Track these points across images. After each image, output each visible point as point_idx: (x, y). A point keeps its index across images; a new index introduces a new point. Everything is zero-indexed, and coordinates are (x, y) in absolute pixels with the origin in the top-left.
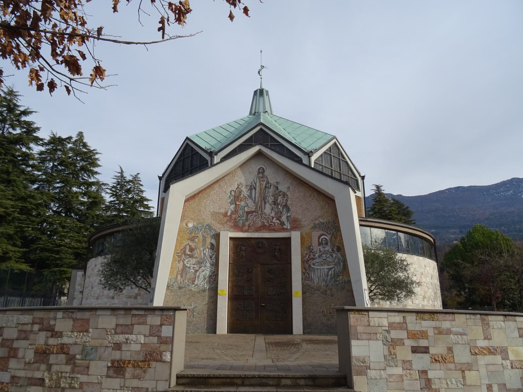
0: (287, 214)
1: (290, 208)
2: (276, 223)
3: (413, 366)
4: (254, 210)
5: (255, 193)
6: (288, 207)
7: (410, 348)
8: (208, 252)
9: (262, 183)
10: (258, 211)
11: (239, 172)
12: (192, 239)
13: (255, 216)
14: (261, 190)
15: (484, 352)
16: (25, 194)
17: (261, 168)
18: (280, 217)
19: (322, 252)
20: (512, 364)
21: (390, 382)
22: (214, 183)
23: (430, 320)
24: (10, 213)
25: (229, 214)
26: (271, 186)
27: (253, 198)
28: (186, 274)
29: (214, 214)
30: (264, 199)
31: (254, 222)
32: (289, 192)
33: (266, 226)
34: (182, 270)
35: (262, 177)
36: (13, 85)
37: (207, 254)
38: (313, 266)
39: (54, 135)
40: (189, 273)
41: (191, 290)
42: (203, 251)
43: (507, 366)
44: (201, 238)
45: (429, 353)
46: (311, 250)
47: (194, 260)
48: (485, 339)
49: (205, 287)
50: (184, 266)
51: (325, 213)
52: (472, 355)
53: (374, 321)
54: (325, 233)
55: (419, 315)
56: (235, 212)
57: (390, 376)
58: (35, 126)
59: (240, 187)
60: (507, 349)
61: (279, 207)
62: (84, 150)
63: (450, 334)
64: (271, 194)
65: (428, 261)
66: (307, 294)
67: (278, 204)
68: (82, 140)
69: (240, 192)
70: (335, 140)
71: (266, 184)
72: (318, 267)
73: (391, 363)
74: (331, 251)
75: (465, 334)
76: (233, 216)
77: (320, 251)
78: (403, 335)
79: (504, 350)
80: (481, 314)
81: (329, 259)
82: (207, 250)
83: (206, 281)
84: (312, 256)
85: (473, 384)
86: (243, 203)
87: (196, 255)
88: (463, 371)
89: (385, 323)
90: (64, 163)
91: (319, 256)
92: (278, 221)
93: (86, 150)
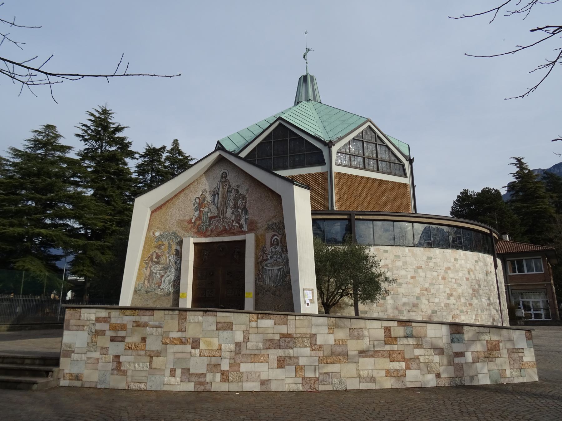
0: (246, 216)
1: (248, 210)
2: (236, 227)
3: (109, 352)
4: (216, 215)
5: (218, 198)
6: (247, 209)
7: (109, 337)
8: (173, 258)
9: (225, 187)
10: (220, 216)
11: (204, 179)
12: (159, 247)
13: (218, 220)
14: (223, 195)
15: (175, 342)
16: (122, 208)
17: (224, 172)
18: (240, 220)
19: (273, 253)
20: (201, 352)
21: (88, 363)
22: (180, 192)
23: (131, 315)
24: (108, 226)
25: (193, 221)
26: (232, 189)
27: (216, 203)
28: (153, 280)
29: (180, 222)
30: (226, 203)
31: (216, 227)
32: (247, 195)
33: (226, 229)
34: (149, 276)
35: (225, 182)
36: (106, 104)
37: (172, 260)
38: (265, 267)
39: (149, 146)
40: (155, 278)
41: (157, 294)
42: (169, 257)
43: (195, 354)
44: (167, 245)
45: (124, 342)
46: (264, 251)
47: (160, 266)
48: (179, 331)
49: (170, 290)
50: (151, 272)
51: (278, 213)
52: (163, 344)
53: (84, 316)
54: (277, 234)
55: (123, 311)
56: (199, 218)
57: (89, 358)
58: (126, 141)
59: (204, 193)
60: (200, 340)
61: (239, 210)
62: (180, 157)
63: (146, 327)
64: (232, 198)
65: (464, 255)
66: (260, 295)
67: (238, 207)
68: (178, 148)
69: (204, 199)
70: (369, 124)
71: (228, 189)
72: (270, 268)
73: (91, 348)
74: (281, 252)
75: (160, 327)
76: (197, 222)
77: (272, 252)
78: (106, 327)
79: (196, 341)
80: (203, 311)
81: (278, 260)
82: (172, 256)
83: (171, 285)
84: (265, 257)
85: (158, 368)
86: (206, 209)
87: (162, 262)
88: (151, 357)
89: (93, 317)
90: (159, 173)
91: (271, 257)
92: (237, 225)
93: (182, 158)
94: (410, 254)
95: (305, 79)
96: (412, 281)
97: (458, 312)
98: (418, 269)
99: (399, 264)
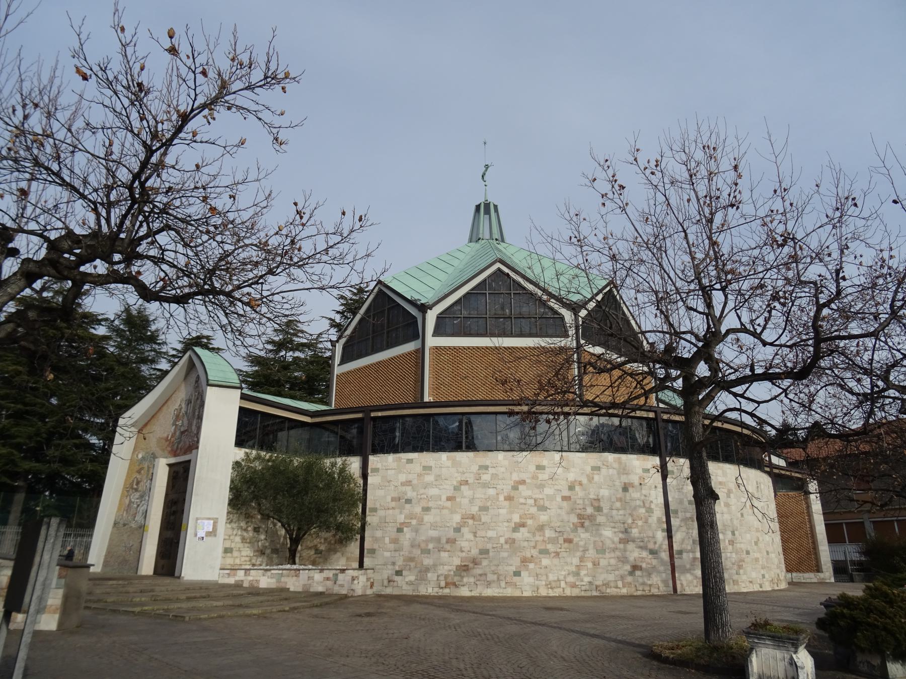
12: (139, 472)
65: (448, 458)
94: (449, 463)
95: (485, 209)
96: (449, 504)
97: (535, 552)
98: (461, 485)
99: (430, 478)
